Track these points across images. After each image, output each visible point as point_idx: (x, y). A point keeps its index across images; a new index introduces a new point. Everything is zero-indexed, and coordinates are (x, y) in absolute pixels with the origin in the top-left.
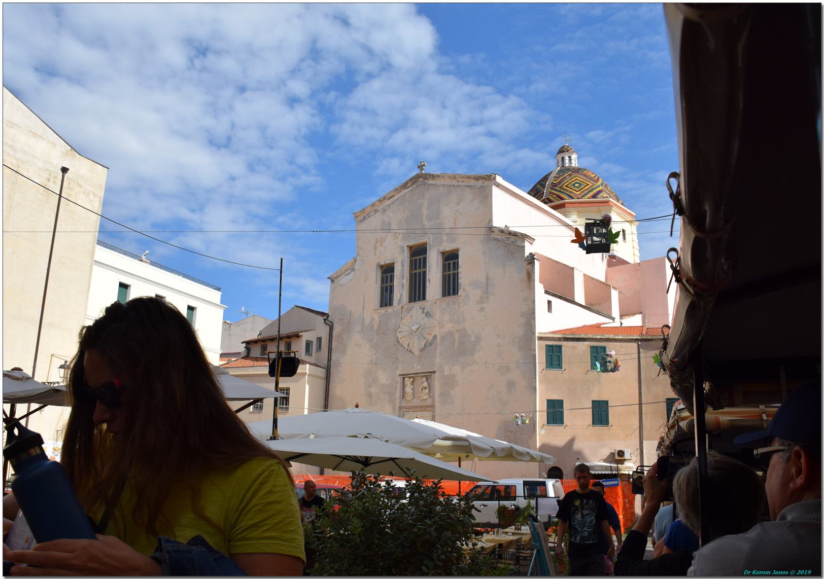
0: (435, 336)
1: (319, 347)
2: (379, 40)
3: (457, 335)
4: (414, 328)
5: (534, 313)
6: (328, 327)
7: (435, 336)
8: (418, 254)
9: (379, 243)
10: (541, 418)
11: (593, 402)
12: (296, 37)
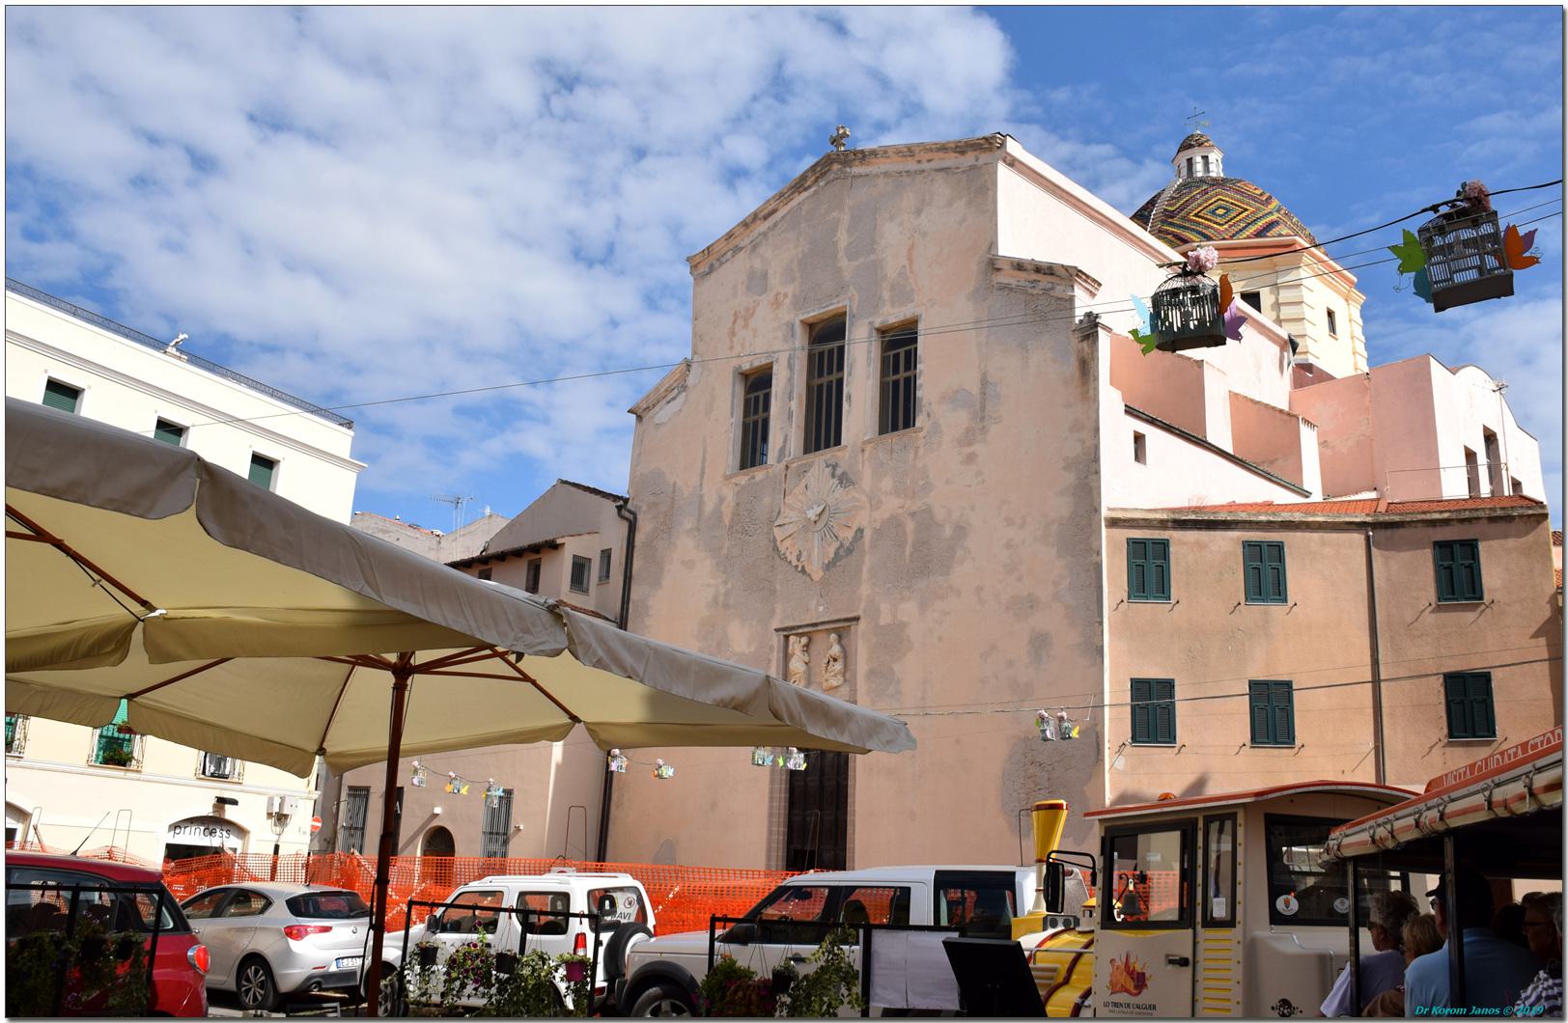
0: (860, 531)
1: (606, 575)
2: (900, 61)
3: (910, 526)
4: (812, 514)
5: (1096, 460)
6: (625, 526)
7: (860, 531)
8: (826, 338)
9: (741, 322)
10: (1116, 723)
11: (1253, 684)
12: (746, 58)
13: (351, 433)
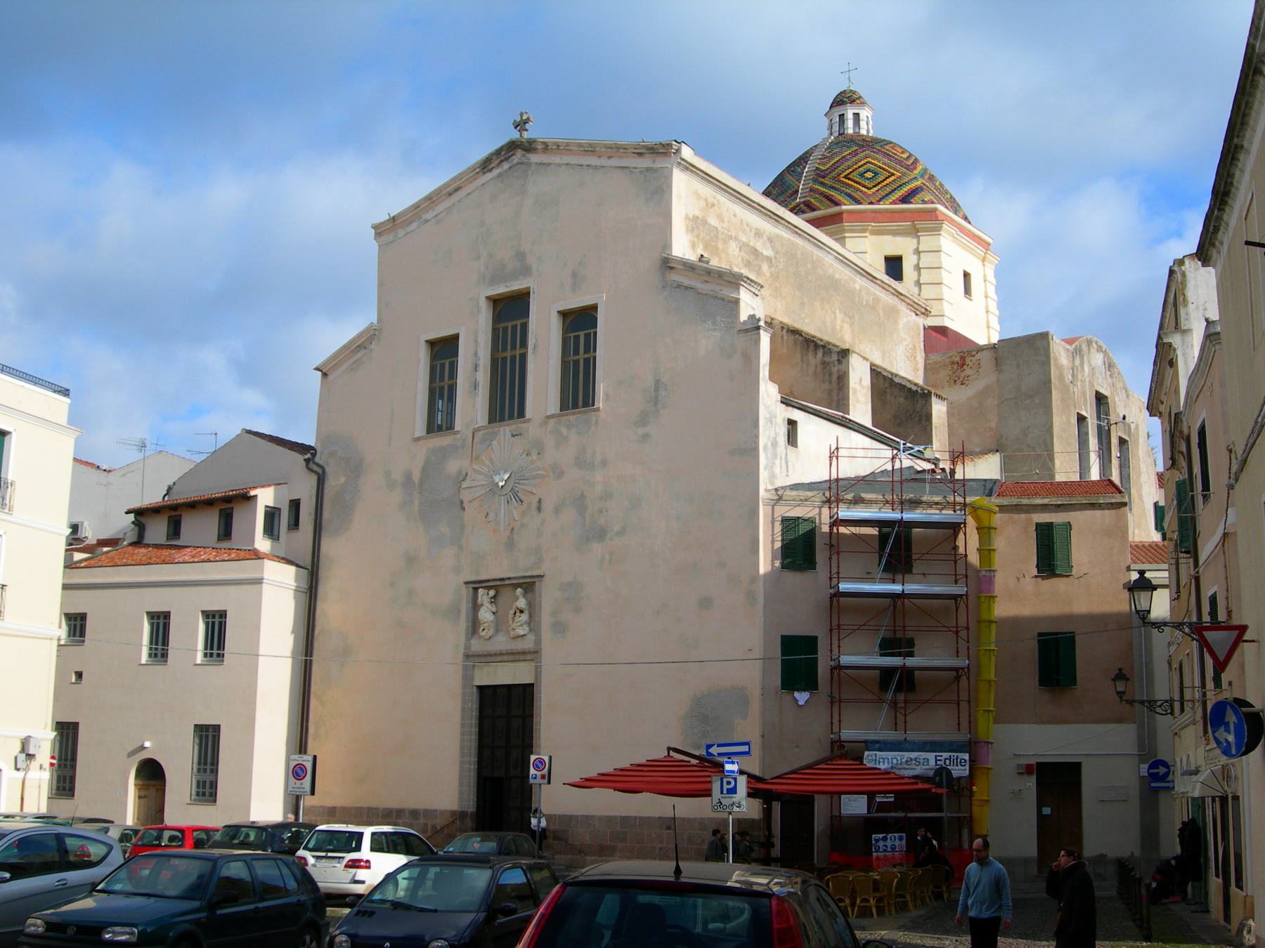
1: (295, 524)
6: (314, 478)
8: (510, 310)
13: (67, 400)
